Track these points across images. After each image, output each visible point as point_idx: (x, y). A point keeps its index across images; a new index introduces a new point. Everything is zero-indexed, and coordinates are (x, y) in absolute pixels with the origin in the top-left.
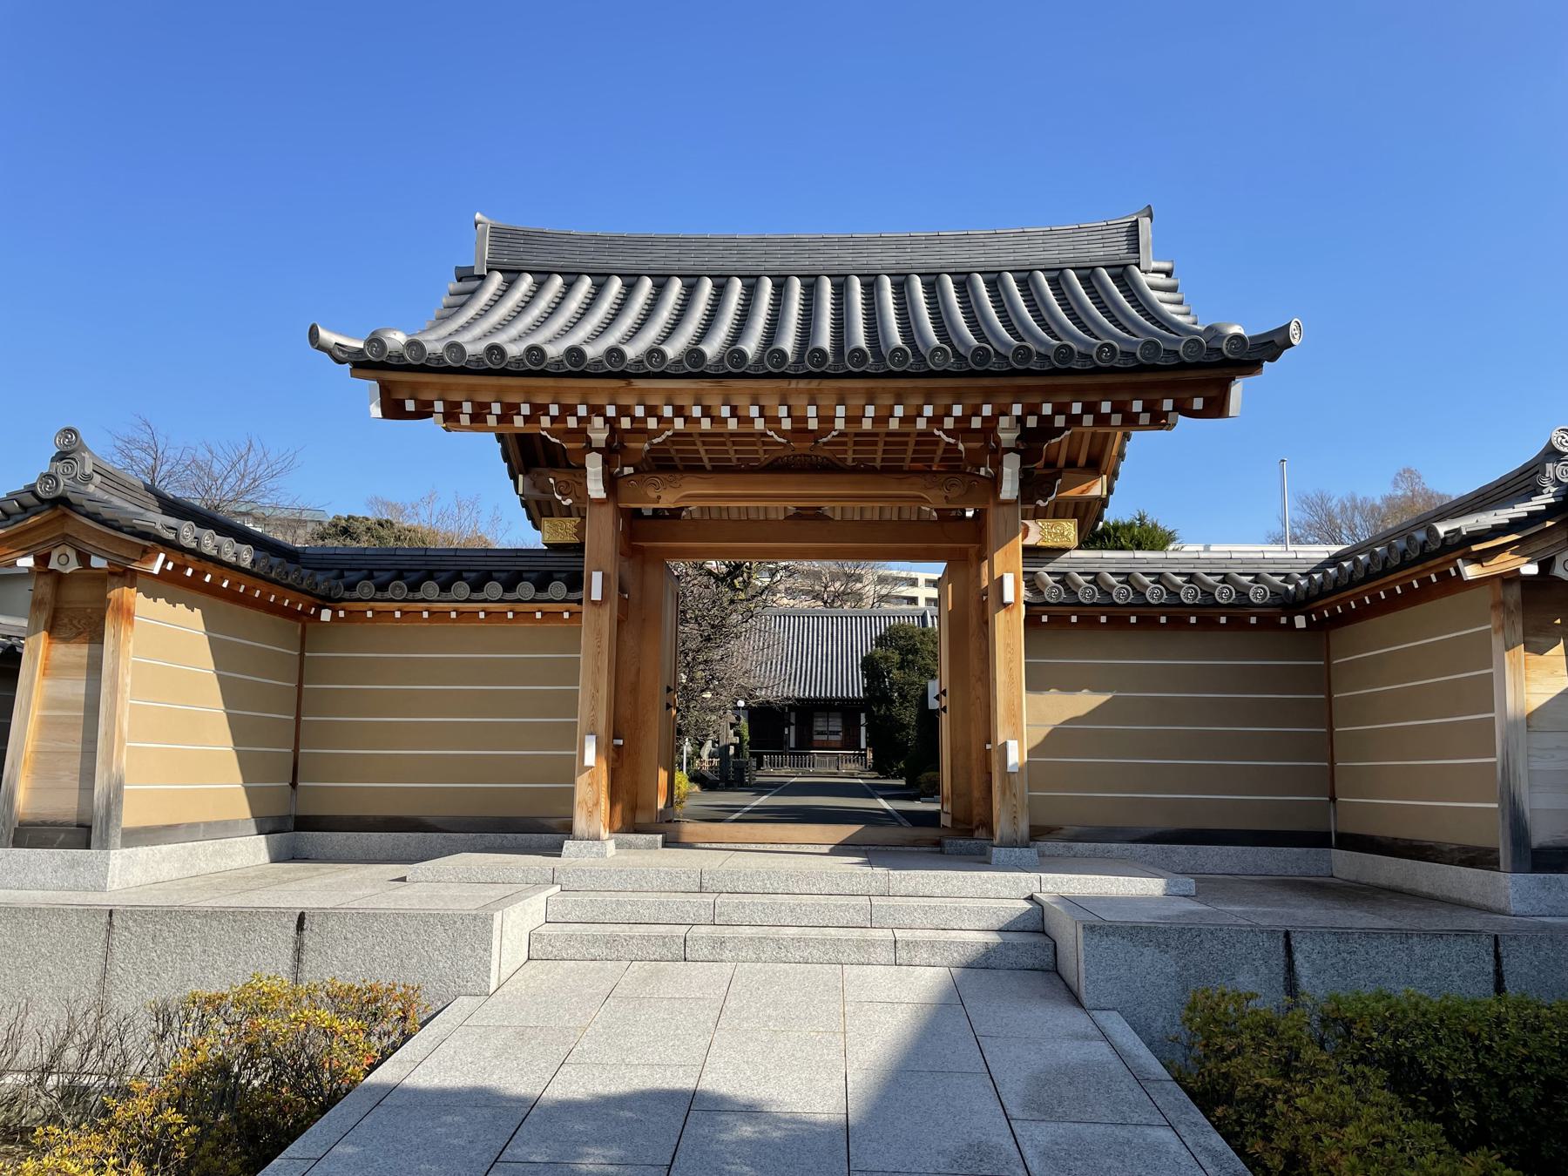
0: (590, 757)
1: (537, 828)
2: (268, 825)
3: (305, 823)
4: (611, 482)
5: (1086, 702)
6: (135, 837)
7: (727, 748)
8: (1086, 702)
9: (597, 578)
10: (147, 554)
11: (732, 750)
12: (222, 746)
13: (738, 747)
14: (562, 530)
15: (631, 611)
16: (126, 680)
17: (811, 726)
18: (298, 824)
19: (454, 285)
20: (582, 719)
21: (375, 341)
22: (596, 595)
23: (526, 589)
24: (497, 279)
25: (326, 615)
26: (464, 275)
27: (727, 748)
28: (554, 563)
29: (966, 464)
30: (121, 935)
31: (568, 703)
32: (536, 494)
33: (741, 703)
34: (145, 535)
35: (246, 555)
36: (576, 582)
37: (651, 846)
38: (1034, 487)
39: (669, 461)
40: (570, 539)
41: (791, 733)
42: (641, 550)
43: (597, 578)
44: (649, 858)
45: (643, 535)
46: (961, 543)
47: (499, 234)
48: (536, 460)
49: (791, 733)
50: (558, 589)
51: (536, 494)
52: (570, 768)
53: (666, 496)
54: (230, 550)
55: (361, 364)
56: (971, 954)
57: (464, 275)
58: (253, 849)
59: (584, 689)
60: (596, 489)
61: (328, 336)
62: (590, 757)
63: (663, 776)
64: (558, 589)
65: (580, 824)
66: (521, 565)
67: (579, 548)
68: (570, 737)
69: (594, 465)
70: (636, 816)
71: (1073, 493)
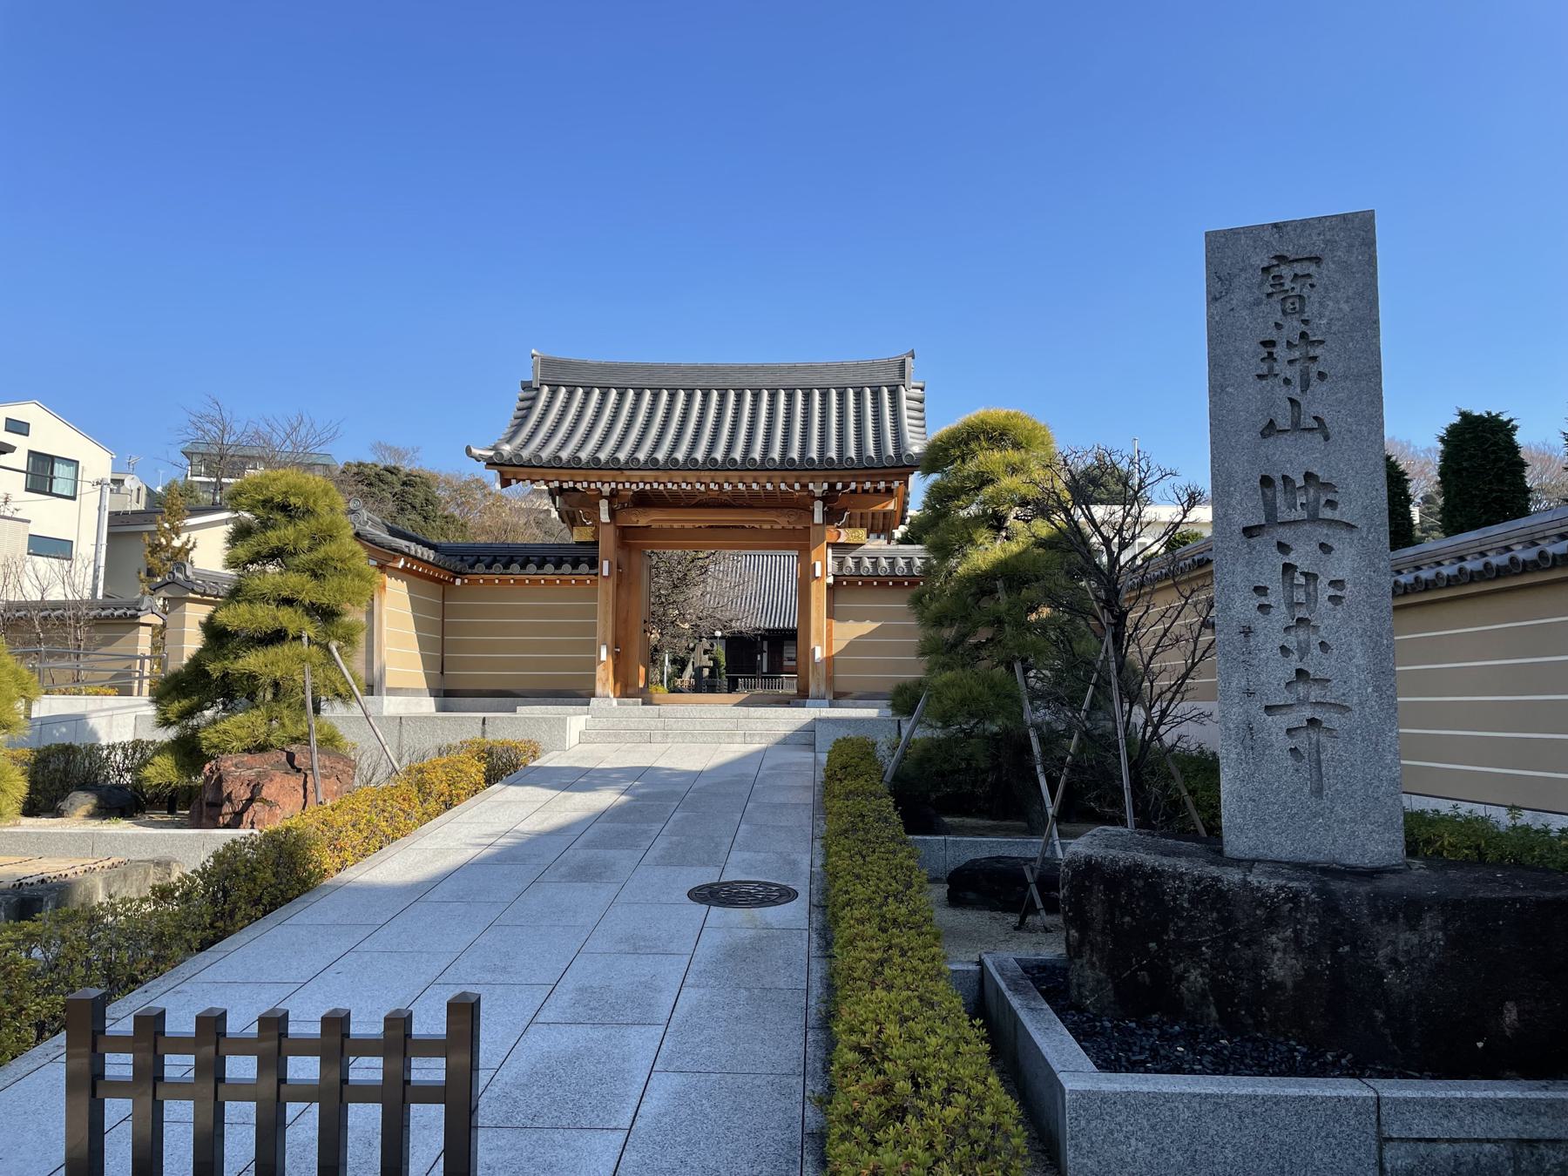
0: (604, 656)
1: (580, 694)
2: (435, 693)
3: (448, 694)
4: (612, 513)
5: (868, 626)
6: (393, 691)
7: (701, 669)
8: (868, 626)
9: (606, 564)
10: (395, 559)
11: (706, 672)
12: (415, 650)
13: (712, 671)
14: (581, 535)
15: (623, 579)
16: (385, 617)
17: (781, 653)
18: (447, 693)
19: (522, 394)
20: (599, 638)
21: (499, 453)
22: (605, 573)
23: (567, 568)
24: (546, 389)
25: (458, 582)
26: (526, 386)
27: (701, 669)
28: (580, 552)
29: (801, 506)
30: (405, 727)
31: (592, 629)
32: (567, 507)
33: (718, 634)
34: (396, 550)
35: (429, 555)
36: (594, 563)
37: (636, 704)
38: (832, 517)
39: (644, 500)
40: (590, 539)
41: (764, 660)
42: (628, 545)
43: (606, 564)
44: (635, 708)
45: (627, 537)
46: (801, 542)
47: (547, 363)
48: (574, 504)
49: (764, 660)
50: (584, 568)
51: (567, 507)
52: (593, 664)
53: (642, 519)
54: (421, 551)
55: (491, 463)
56: (778, 738)
57: (526, 386)
58: (427, 705)
59: (599, 622)
60: (605, 518)
61: (476, 451)
62: (604, 656)
63: (642, 670)
64: (584, 568)
65: (599, 690)
66: (562, 553)
67: (596, 543)
68: (595, 650)
69: (604, 506)
70: (626, 688)
71: (878, 508)
